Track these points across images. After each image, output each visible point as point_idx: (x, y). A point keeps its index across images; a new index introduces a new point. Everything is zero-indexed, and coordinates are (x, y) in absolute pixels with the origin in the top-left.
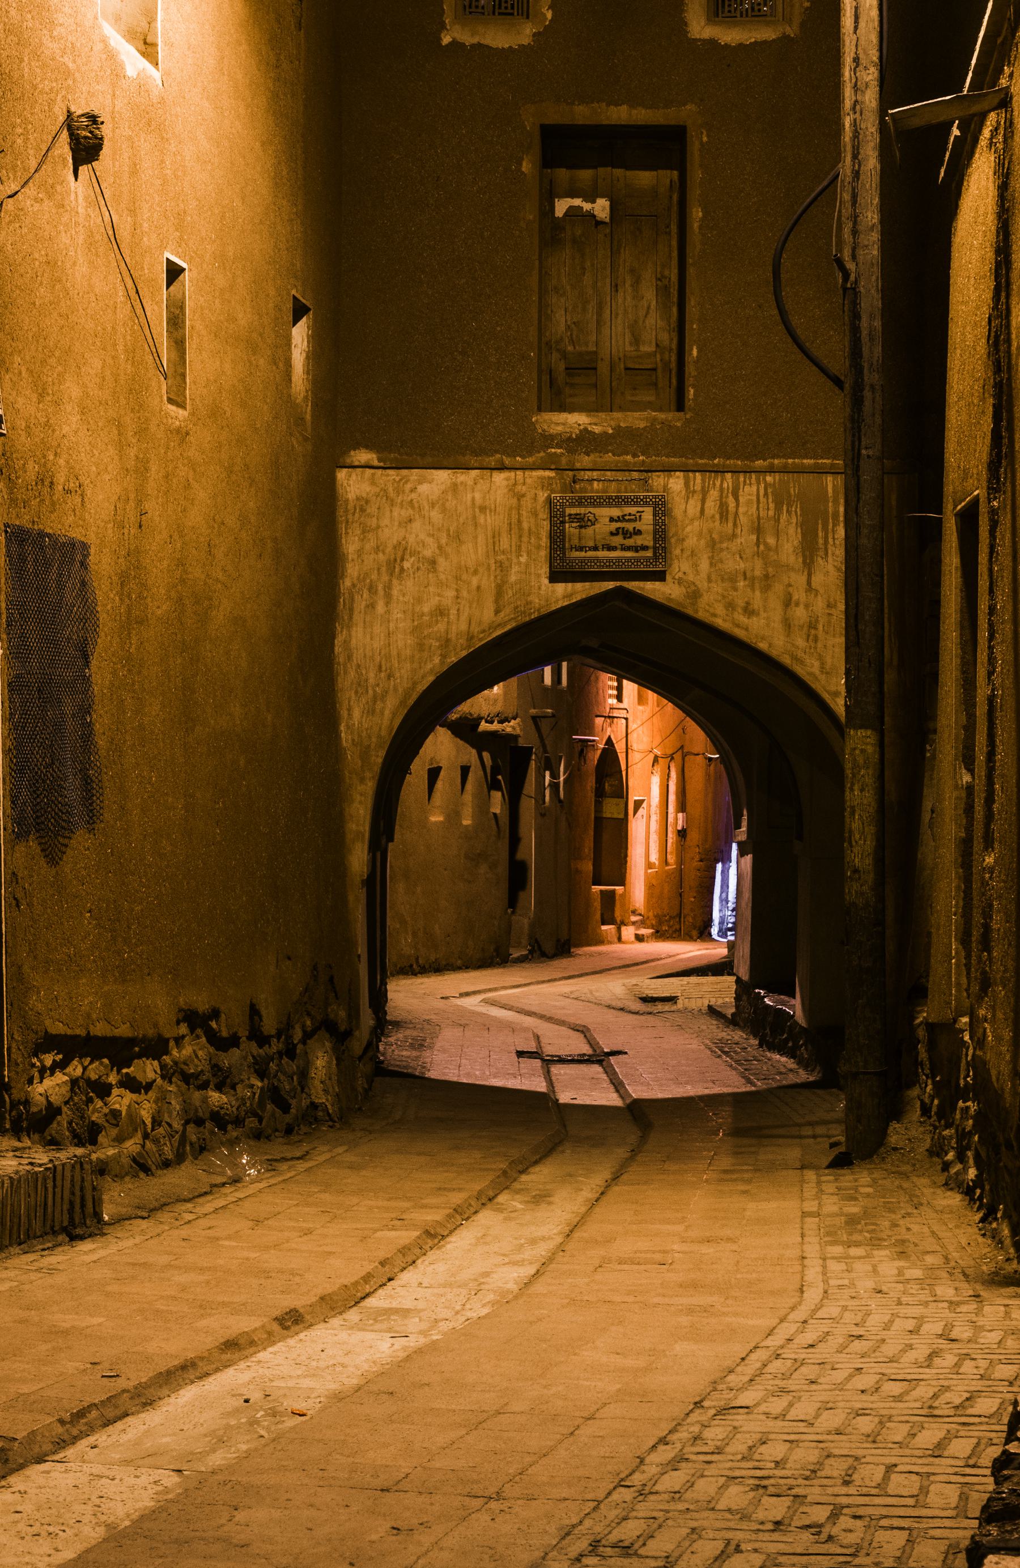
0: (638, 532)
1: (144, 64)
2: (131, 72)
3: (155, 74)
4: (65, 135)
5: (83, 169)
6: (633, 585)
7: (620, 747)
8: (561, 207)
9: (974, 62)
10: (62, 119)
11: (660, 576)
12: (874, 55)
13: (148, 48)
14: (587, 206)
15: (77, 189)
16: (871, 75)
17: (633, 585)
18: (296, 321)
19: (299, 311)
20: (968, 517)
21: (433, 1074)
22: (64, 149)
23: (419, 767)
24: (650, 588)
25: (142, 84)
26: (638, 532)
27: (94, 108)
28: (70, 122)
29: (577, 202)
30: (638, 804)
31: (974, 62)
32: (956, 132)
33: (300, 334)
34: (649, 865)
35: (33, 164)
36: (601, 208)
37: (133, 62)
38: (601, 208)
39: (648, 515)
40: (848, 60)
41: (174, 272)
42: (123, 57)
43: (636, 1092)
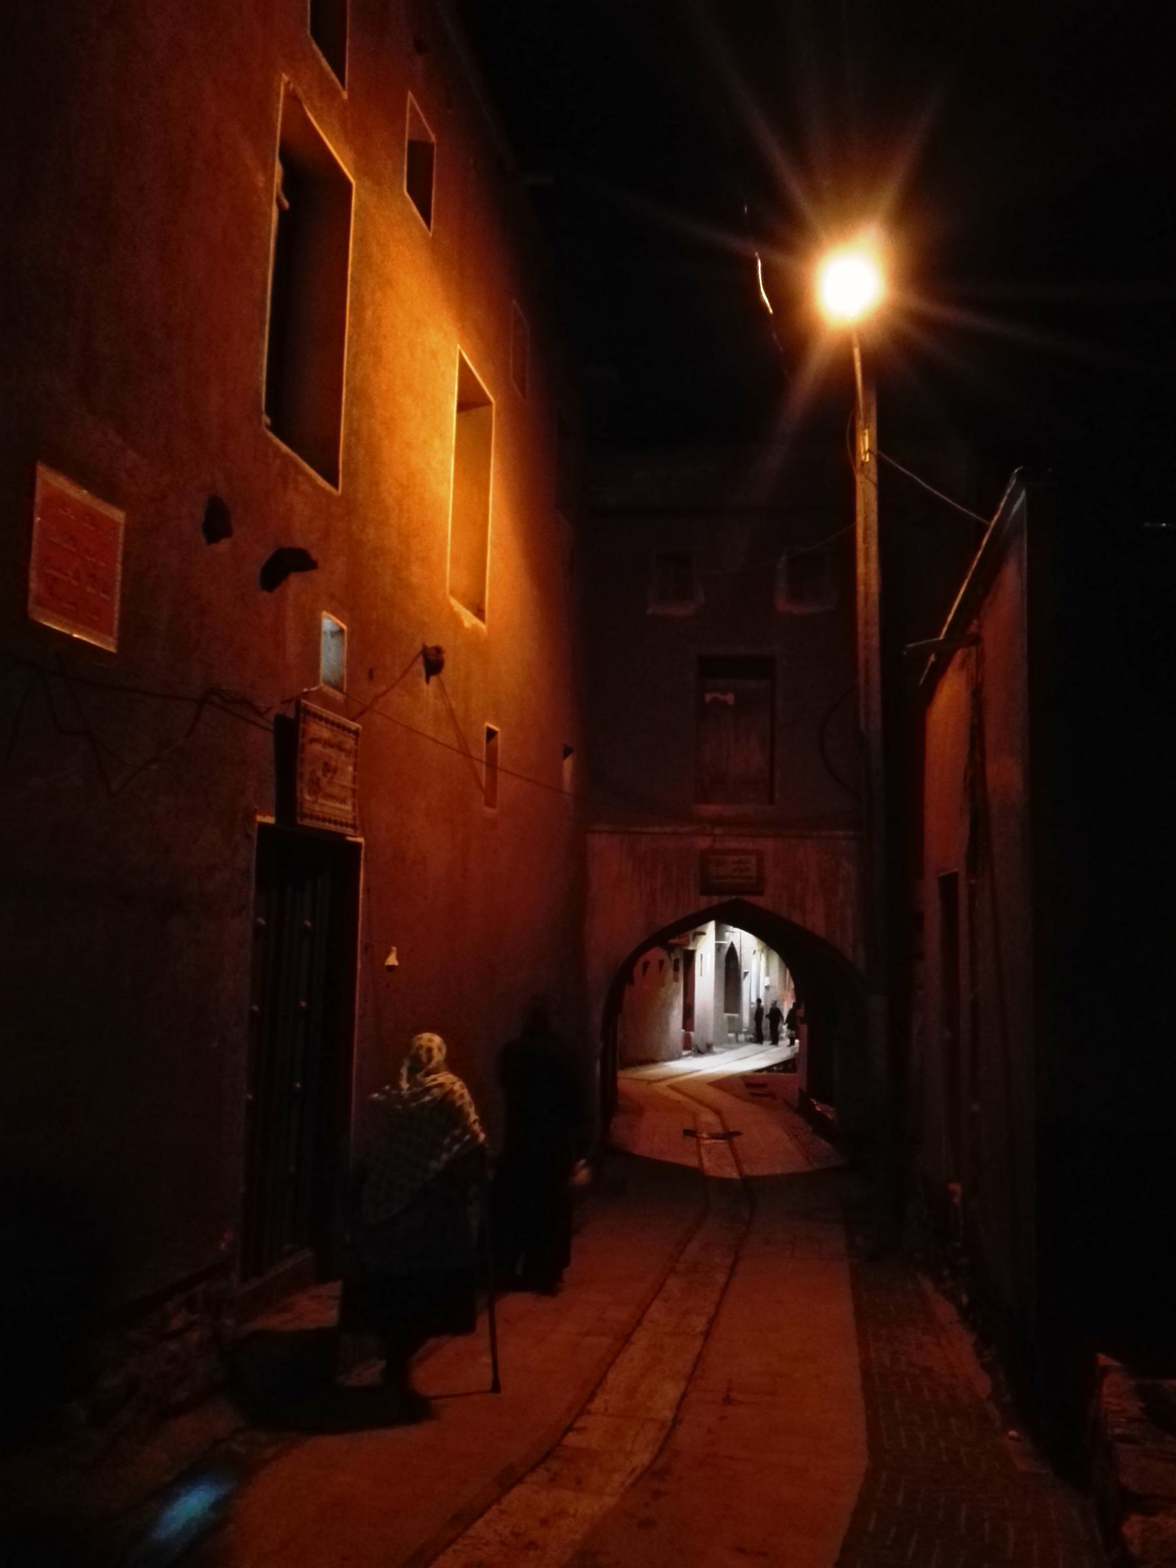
0: (747, 869)
1: (476, 621)
2: (467, 624)
3: (483, 626)
4: (421, 659)
5: (433, 679)
6: (746, 898)
7: (737, 947)
8: (709, 697)
9: (950, 618)
10: (420, 648)
11: (761, 893)
12: (877, 620)
13: (479, 613)
14: (722, 697)
15: (428, 689)
16: (875, 630)
17: (746, 898)
18: (566, 755)
19: (567, 752)
20: (949, 884)
21: (637, 1152)
22: (420, 667)
23: (641, 960)
24: (753, 899)
25: (475, 630)
26: (747, 869)
27: (441, 644)
28: (425, 652)
29: (717, 695)
30: (746, 974)
31: (950, 618)
32: (932, 658)
33: (568, 763)
34: (751, 1003)
35: (398, 675)
36: (730, 698)
37: (469, 619)
38: (730, 698)
39: (753, 860)
40: (861, 622)
41: (491, 734)
42: (463, 617)
43: (748, 1170)
